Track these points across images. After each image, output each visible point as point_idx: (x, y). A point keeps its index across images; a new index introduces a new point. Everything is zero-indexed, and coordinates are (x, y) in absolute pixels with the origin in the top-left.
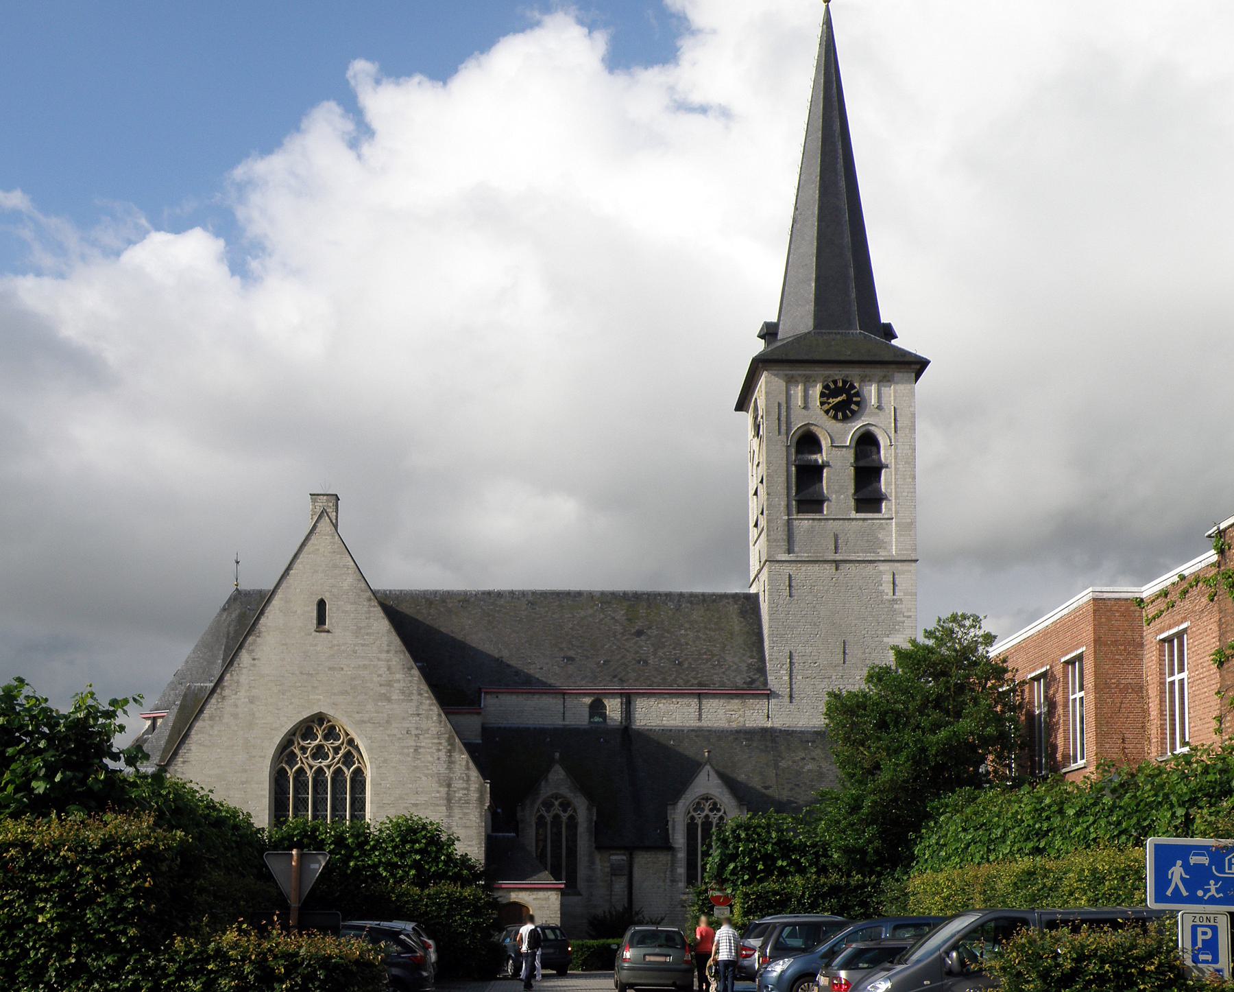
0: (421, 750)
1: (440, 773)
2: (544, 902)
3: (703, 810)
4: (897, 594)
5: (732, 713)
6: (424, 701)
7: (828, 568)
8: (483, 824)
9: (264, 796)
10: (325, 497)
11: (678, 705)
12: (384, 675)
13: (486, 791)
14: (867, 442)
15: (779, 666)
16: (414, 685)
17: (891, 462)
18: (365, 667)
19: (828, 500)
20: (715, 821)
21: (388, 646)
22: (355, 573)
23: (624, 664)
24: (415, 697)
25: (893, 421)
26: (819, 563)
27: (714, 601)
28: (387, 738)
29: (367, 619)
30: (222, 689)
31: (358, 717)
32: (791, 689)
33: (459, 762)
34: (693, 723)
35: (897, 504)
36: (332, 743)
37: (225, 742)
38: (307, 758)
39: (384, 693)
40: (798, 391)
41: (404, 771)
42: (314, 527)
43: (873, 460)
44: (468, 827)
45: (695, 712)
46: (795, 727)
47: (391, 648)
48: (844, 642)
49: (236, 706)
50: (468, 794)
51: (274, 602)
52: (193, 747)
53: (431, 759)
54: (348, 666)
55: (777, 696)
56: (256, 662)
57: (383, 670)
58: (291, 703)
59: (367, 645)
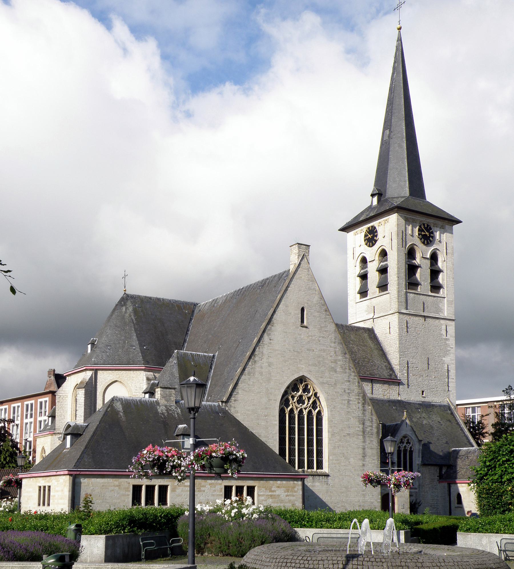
0: (351, 402)
1: (359, 416)
3: (403, 443)
5: (385, 391)
6: (352, 374)
7: (421, 319)
10: (304, 247)
12: (333, 356)
14: (434, 257)
16: (347, 364)
18: (324, 351)
19: (421, 284)
20: (409, 449)
22: (319, 294)
24: (347, 371)
27: (356, 330)
28: (335, 394)
29: (325, 322)
30: (254, 356)
31: (321, 380)
32: (408, 381)
33: (368, 411)
35: (447, 291)
37: (257, 389)
38: (295, 403)
39: (333, 367)
40: (410, 228)
44: (373, 448)
45: (370, 389)
47: (337, 341)
48: (428, 358)
49: (262, 367)
50: (372, 429)
52: (240, 391)
53: (355, 408)
54: (316, 349)
55: (403, 384)
56: (271, 341)
57: (332, 353)
58: (289, 369)
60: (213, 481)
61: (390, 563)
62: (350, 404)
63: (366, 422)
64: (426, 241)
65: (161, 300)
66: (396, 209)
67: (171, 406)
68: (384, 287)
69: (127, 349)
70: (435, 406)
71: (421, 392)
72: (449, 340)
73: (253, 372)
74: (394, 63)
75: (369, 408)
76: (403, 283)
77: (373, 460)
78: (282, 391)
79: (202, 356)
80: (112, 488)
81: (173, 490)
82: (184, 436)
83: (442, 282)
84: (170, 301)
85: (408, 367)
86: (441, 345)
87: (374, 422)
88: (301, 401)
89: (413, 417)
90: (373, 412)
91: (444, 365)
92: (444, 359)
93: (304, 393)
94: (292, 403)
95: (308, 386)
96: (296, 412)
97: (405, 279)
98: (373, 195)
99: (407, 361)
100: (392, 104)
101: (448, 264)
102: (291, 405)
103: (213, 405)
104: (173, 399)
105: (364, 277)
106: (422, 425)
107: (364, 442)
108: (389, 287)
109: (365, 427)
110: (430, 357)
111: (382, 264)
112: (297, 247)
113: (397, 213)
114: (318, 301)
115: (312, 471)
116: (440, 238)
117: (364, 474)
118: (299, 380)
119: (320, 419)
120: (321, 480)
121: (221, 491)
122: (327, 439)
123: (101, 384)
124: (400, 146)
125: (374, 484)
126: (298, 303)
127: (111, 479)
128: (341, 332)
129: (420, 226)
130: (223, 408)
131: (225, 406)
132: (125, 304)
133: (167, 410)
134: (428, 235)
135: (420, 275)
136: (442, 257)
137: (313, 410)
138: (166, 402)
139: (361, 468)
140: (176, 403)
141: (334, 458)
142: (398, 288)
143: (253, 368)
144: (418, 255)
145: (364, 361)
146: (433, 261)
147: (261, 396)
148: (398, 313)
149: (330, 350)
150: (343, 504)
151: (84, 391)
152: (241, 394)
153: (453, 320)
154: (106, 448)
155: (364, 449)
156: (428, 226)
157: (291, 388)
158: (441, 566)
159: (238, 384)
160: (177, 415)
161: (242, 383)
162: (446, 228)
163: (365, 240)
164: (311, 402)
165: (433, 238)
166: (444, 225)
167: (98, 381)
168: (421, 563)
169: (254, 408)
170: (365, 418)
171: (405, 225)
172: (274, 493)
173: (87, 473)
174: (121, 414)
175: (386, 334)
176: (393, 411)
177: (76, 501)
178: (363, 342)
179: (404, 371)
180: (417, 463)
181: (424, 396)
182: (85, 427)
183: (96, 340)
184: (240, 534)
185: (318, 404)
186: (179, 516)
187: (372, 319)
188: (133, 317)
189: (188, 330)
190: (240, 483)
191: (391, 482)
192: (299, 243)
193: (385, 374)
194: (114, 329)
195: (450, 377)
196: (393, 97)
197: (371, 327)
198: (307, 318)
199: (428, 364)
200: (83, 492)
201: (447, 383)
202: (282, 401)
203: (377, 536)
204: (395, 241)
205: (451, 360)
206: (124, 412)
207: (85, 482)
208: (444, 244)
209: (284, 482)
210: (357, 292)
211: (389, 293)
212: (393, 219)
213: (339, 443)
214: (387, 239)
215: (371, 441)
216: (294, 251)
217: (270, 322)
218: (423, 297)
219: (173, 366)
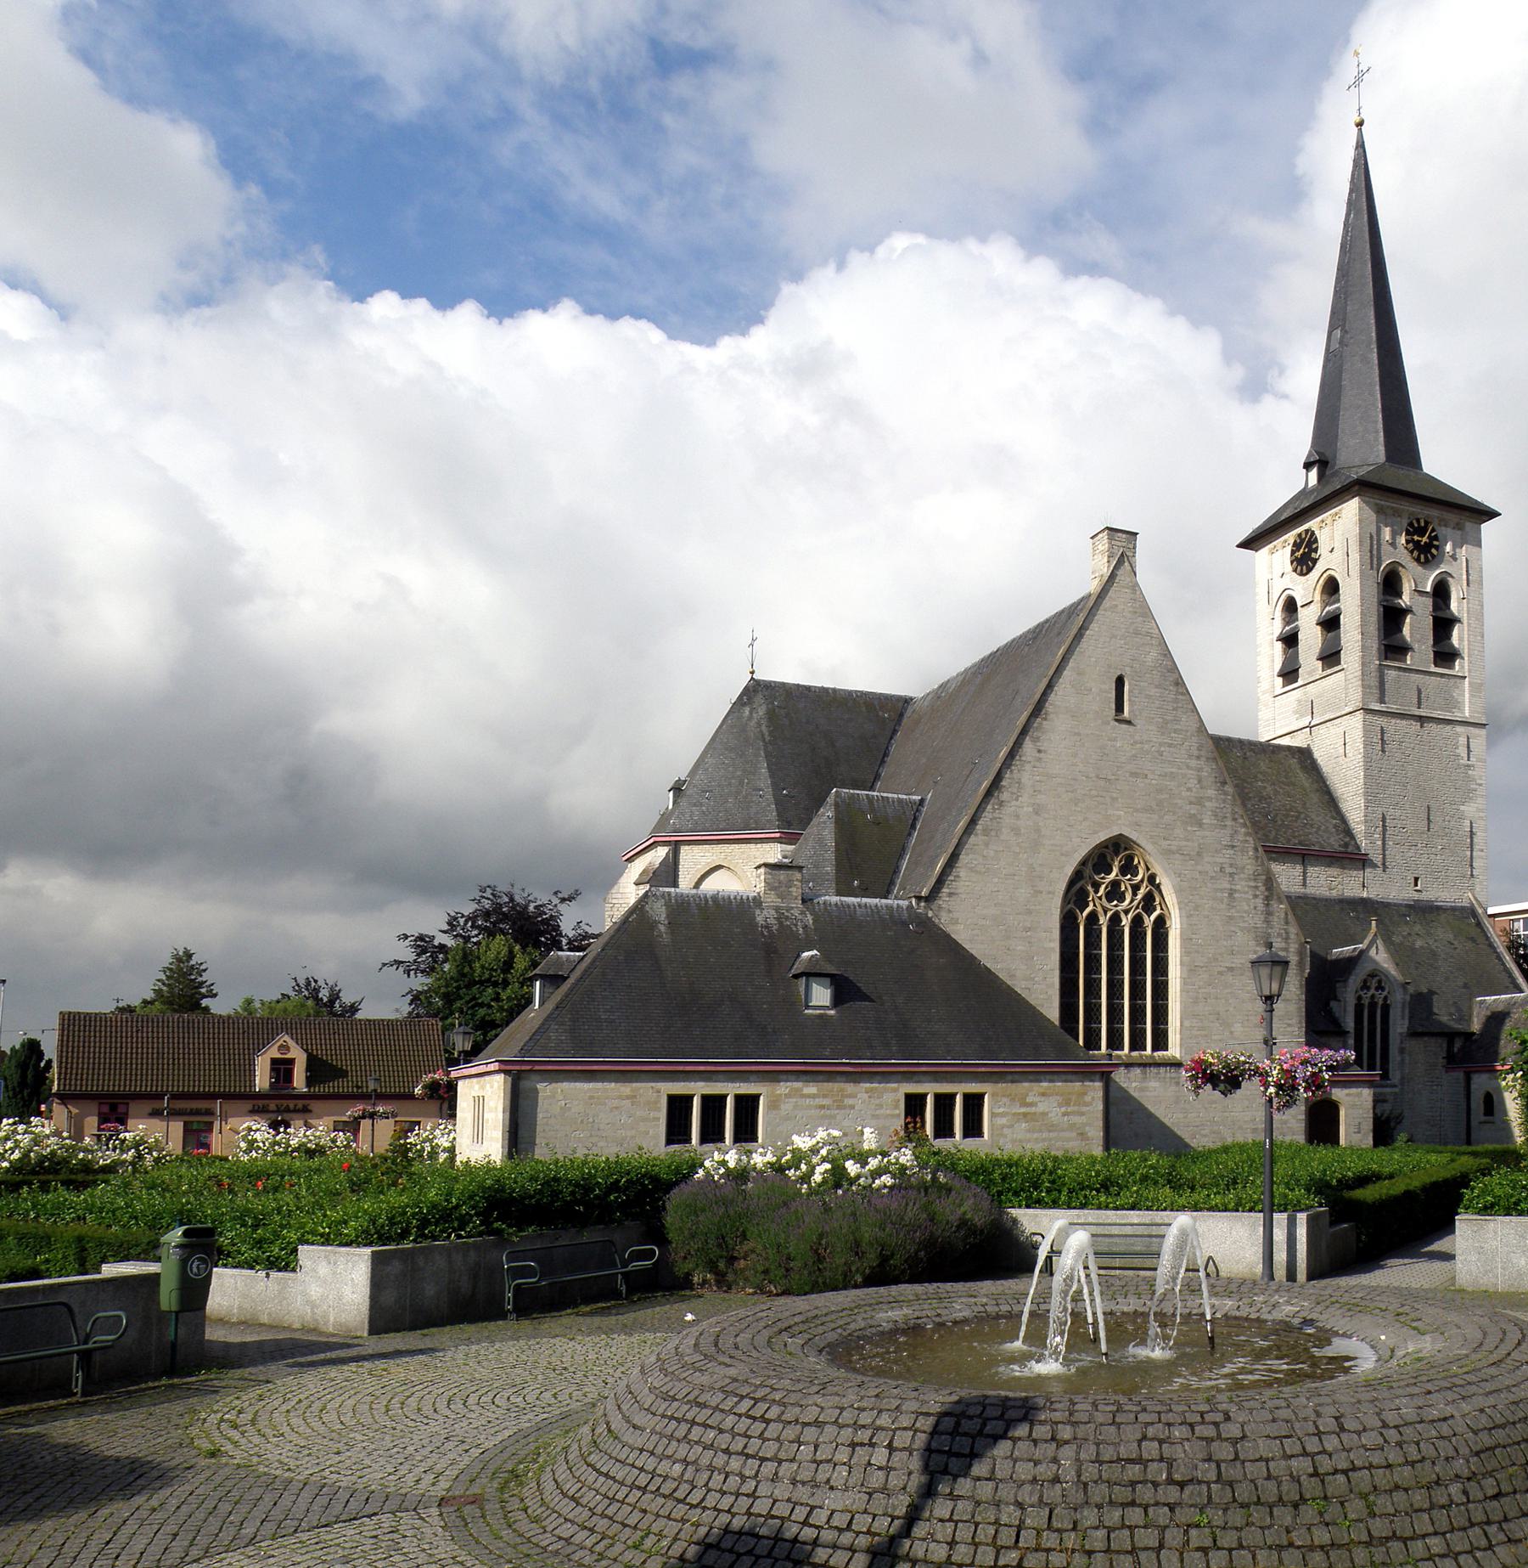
0: (1236, 895)
2: (1356, 1099)
3: (1368, 988)
9: (1053, 949)
10: (1124, 536)
12: (1194, 790)
14: (1441, 592)
20: (1381, 1002)
22: (1160, 644)
24: (1229, 823)
25: (1465, 572)
27: (1273, 752)
32: (1384, 858)
35: (1470, 662)
38: (1100, 898)
40: (1387, 533)
42: (1112, 576)
47: (1202, 753)
48: (1428, 807)
49: (1017, 817)
52: (963, 873)
53: (1246, 908)
54: (1153, 772)
55: (1375, 866)
56: (1042, 755)
57: (1193, 783)
58: (1085, 819)
59: (1175, 746)
61: (1093, 1448)
64: (1422, 556)
66: (1356, 488)
68: (1330, 659)
69: (746, 797)
76: (1374, 645)
77: (1289, 1025)
78: (1069, 871)
79: (893, 802)
80: (616, 1103)
81: (773, 1105)
82: (811, 979)
85: (1384, 826)
88: (1115, 893)
89: (1393, 933)
92: (1462, 808)
95: (1133, 860)
96: (1103, 921)
98: (1308, 466)
101: (1470, 605)
102: (1091, 904)
103: (895, 906)
104: (796, 891)
105: (1290, 641)
106: (1413, 949)
108: (1342, 656)
115: (1141, 1056)
117: (1192, 1061)
120: (1163, 1075)
121: (896, 1107)
122: (1178, 980)
124: (1365, 360)
125: (1222, 1086)
126: (1109, 666)
132: (750, 702)
135: (1411, 630)
136: (1457, 590)
140: (804, 901)
142: (1363, 657)
143: (996, 818)
144: (1407, 587)
145: (1287, 816)
149: (1186, 775)
150: (1216, 1128)
152: (964, 879)
157: (1090, 865)
158: (1324, 1452)
159: (959, 855)
163: (1292, 563)
164: (1139, 897)
165: (1437, 540)
168: (1234, 1442)
174: (662, 928)
176: (1348, 922)
177: (522, 1133)
180: (1399, 1030)
184: (821, 1236)
185: (1157, 900)
186: (669, 1186)
188: (764, 728)
189: (886, 755)
191: (1270, 1079)
193: (1334, 843)
195: (1476, 847)
198: (1130, 700)
202: (1070, 895)
203: (1231, 1229)
204: (1355, 556)
210: (1276, 674)
212: (1351, 508)
214: (1339, 554)
216: (1100, 547)
219: (825, 823)
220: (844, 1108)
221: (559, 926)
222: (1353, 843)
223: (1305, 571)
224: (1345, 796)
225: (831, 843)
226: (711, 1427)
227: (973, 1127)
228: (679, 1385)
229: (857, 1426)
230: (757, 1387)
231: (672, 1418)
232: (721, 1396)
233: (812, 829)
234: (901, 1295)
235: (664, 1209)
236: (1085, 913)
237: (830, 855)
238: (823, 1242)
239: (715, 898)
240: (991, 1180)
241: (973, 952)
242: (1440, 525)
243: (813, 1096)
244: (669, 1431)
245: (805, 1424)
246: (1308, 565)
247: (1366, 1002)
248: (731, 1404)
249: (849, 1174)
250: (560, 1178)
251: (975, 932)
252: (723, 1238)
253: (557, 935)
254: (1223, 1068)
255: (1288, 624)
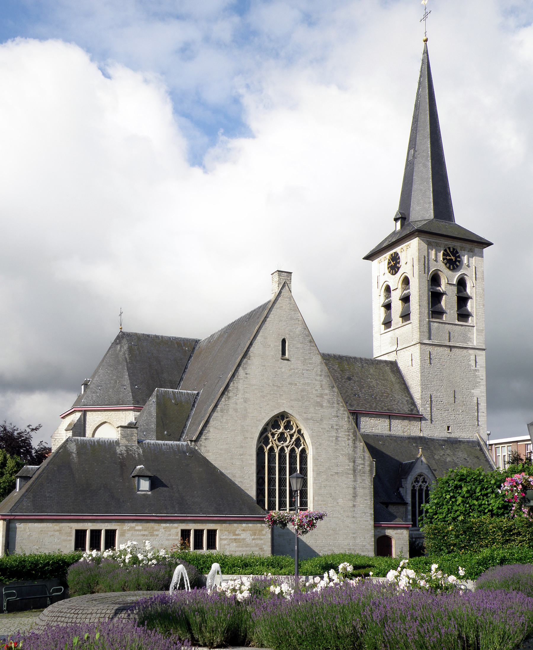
0: (339, 439)
1: (349, 454)
2: (400, 536)
3: (418, 482)
4: (477, 367)
5: (405, 427)
8: (373, 486)
9: (253, 464)
10: (286, 274)
11: (380, 421)
13: (373, 466)
14: (462, 283)
15: (425, 402)
16: (335, 398)
17: (473, 296)
18: (308, 384)
19: (446, 313)
20: (425, 488)
21: (321, 372)
22: (302, 324)
23: (348, 396)
24: (335, 405)
25: (474, 274)
26: (443, 346)
27: (377, 364)
28: (321, 430)
29: (309, 354)
30: (228, 392)
31: (305, 415)
34: (386, 432)
35: (477, 319)
36: (289, 432)
37: (230, 427)
40: (433, 253)
41: (331, 452)
42: (280, 292)
43: (464, 294)
44: (365, 488)
45: (388, 426)
46: (433, 437)
48: (455, 391)
49: (236, 404)
50: (364, 468)
51: (258, 338)
53: (344, 445)
54: (299, 383)
55: (426, 420)
56: (248, 376)
57: (318, 387)
58: (268, 404)
60: (168, 525)
62: (338, 440)
63: (357, 460)
64: (451, 266)
65: (160, 337)
66: (417, 233)
67: (132, 446)
69: (118, 389)
70: (463, 442)
71: (447, 428)
72: (479, 370)
73: (227, 409)
74: (420, 78)
75: (361, 445)
77: (366, 500)
78: (260, 428)
81: (122, 534)
82: (140, 478)
83: (471, 310)
84: (170, 338)
85: (431, 401)
86: (470, 376)
87: (366, 460)
90: (365, 449)
91: (473, 398)
92: (472, 391)
93: (286, 430)
94: (272, 441)
95: (290, 422)
96: (277, 451)
97: (428, 307)
98: (396, 220)
99: (431, 395)
100: (417, 121)
101: (477, 290)
102: (271, 443)
103: (181, 445)
104: (135, 438)
105: (388, 307)
106: (445, 463)
107: (355, 481)
109: (356, 465)
110: (456, 390)
111: (405, 292)
112: (277, 275)
113: (419, 237)
114: (301, 331)
116: (468, 262)
118: (280, 417)
119: (304, 457)
121: (177, 535)
122: (312, 478)
123: (90, 425)
124: (425, 166)
126: (279, 335)
127: (51, 524)
128: (359, 366)
129: (445, 250)
130: (192, 448)
131: (194, 445)
132: (120, 343)
133: (126, 451)
134: (454, 260)
136: (470, 282)
137: (296, 448)
138: (127, 442)
139: (351, 509)
140: (138, 442)
141: (320, 499)
142: (420, 317)
143: (226, 404)
144: (443, 282)
145: (382, 396)
146: (462, 287)
147: (236, 434)
148: (419, 344)
149: (315, 383)
150: (330, 548)
151: (72, 433)
152: (212, 432)
153: (484, 350)
154: (50, 491)
155: (355, 488)
156: (454, 249)
157: (270, 425)
160: (138, 455)
161: (214, 421)
162: (475, 251)
163: (388, 268)
164: (293, 440)
166: (473, 248)
167: (87, 422)
169: (228, 447)
170: (355, 455)
171: (428, 250)
172: (239, 537)
173: (23, 517)
174: (74, 455)
175: (408, 366)
178: (383, 376)
179: (427, 406)
181: (450, 431)
182: (36, 469)
183: (90, 380)
185: (302, 441)
186: (68, 564)
187: (396, 352)
188: (127, 355)
189: (186, 368)
190: (199, 527)
192: (279, 270)
193: (406, 409)
194: (107, 368)
195: (480, 411)
196: (418, 114)
197: (395, 360)
199: (455, 397)
200: (18, 538)
201: (477, 417)
202: (261, 439)
204: (416, 267)
205: (481, 392)
206: (77, 453)
207: (20, 527)
208: (472, 269)
209: (250, 525)
210: (381, 323)
211: (411, 323)
212: (415, 243)
213: (324, 483)
215: (363, 480)
216: (275, 279)
217: (246, 355)
218: (449, 326)
219: (151, 404)
220: (154, 535)
221: (31, 444)
222: (415, 409)
223: (394, 273)
224: (412, 386)
225: (154, 414)
226: (63, 617)
227: (212, 545)
228: (56, 609)
229: (101, 613)
230: (77, 607)
231: (53, 616)
232: (67, 609)
233: (146, 407)
234: (138, 593)
235: (67, 573)
236: (268, 447)
237: (154, 420)
238: (126, 585)
239: (98, 441)
240: (199, 563)
241: (216, 465)
242: (461, 250)
243: (140, 530)
244: (52, 620)
245: (88, 614)
246: (395, 270)
247: (417, 488)
248: (71, 616)
249: (139, 559)
250: (26, 560)
251: (217, 456)
252: (89, 584)
253: (30, 448)
254: (278, 518)
255: (387, 298)
